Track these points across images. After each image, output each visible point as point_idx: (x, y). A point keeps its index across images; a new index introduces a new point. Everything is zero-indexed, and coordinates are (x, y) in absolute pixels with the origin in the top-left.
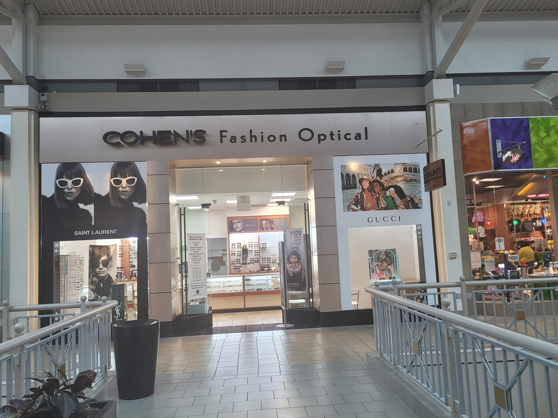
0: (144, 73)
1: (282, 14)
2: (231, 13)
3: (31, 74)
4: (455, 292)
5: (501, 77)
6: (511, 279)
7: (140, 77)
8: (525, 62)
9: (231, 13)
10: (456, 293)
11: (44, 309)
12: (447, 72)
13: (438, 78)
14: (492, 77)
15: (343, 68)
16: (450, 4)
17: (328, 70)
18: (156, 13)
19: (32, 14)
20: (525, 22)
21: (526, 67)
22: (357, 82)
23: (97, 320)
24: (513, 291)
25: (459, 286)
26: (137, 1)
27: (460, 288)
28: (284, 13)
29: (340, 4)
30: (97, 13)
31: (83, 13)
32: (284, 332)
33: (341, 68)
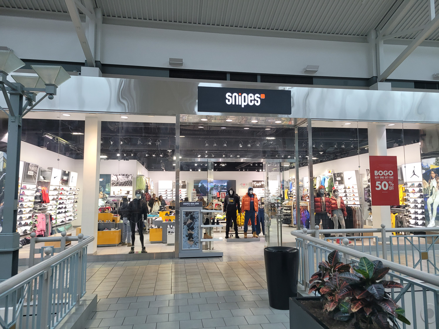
0: (182, 64)
1: (212, 25)
2: (175, 21)
3: (99, 59)
4: (377, 237)
5: (349, 81)
6: (346, 228)
7: (312, 74)
8: (433, 75)
9: (194, 23)
10: (378, 237)
11: (327, 233)
12: (389, 78)
13: (381, 81)
14: (343, 80)
15: (317, 71)
16: (390, 34)
17: (306, 71)
18: (124, 17)
19: (100, 16)
20: (4, 16)
21: (170, 64)
22: (314, 80)
23: (74, 255)
24: (340, 239)
25: (380, 232)
26: (42, 1)
27: (381, 233)
28: (218, 24)
29: (276, 24)
30: (62, 11)
31: (56, 11)
32: (340, 260)
33: (181, 63)
